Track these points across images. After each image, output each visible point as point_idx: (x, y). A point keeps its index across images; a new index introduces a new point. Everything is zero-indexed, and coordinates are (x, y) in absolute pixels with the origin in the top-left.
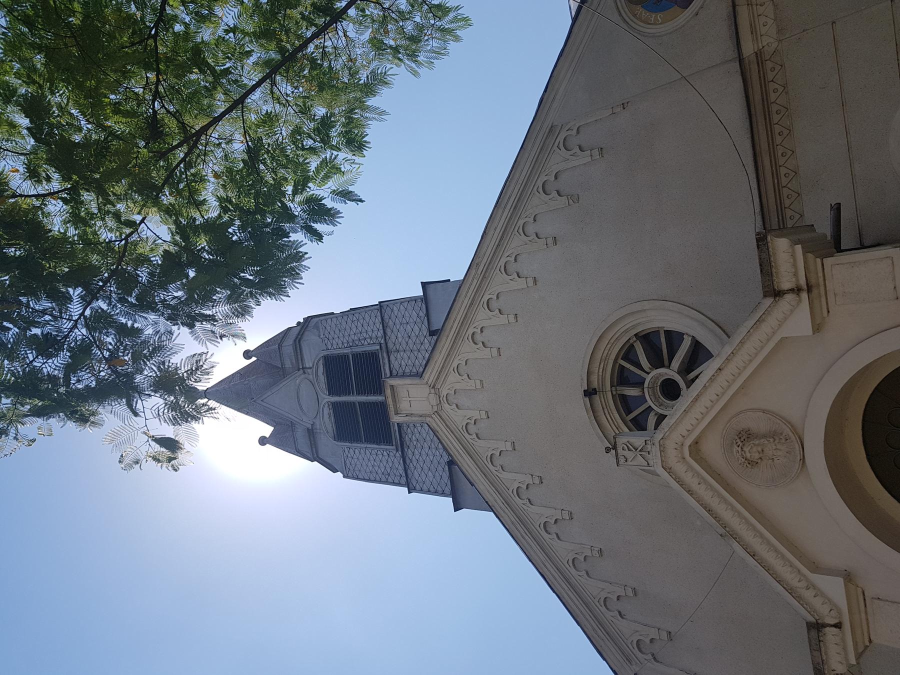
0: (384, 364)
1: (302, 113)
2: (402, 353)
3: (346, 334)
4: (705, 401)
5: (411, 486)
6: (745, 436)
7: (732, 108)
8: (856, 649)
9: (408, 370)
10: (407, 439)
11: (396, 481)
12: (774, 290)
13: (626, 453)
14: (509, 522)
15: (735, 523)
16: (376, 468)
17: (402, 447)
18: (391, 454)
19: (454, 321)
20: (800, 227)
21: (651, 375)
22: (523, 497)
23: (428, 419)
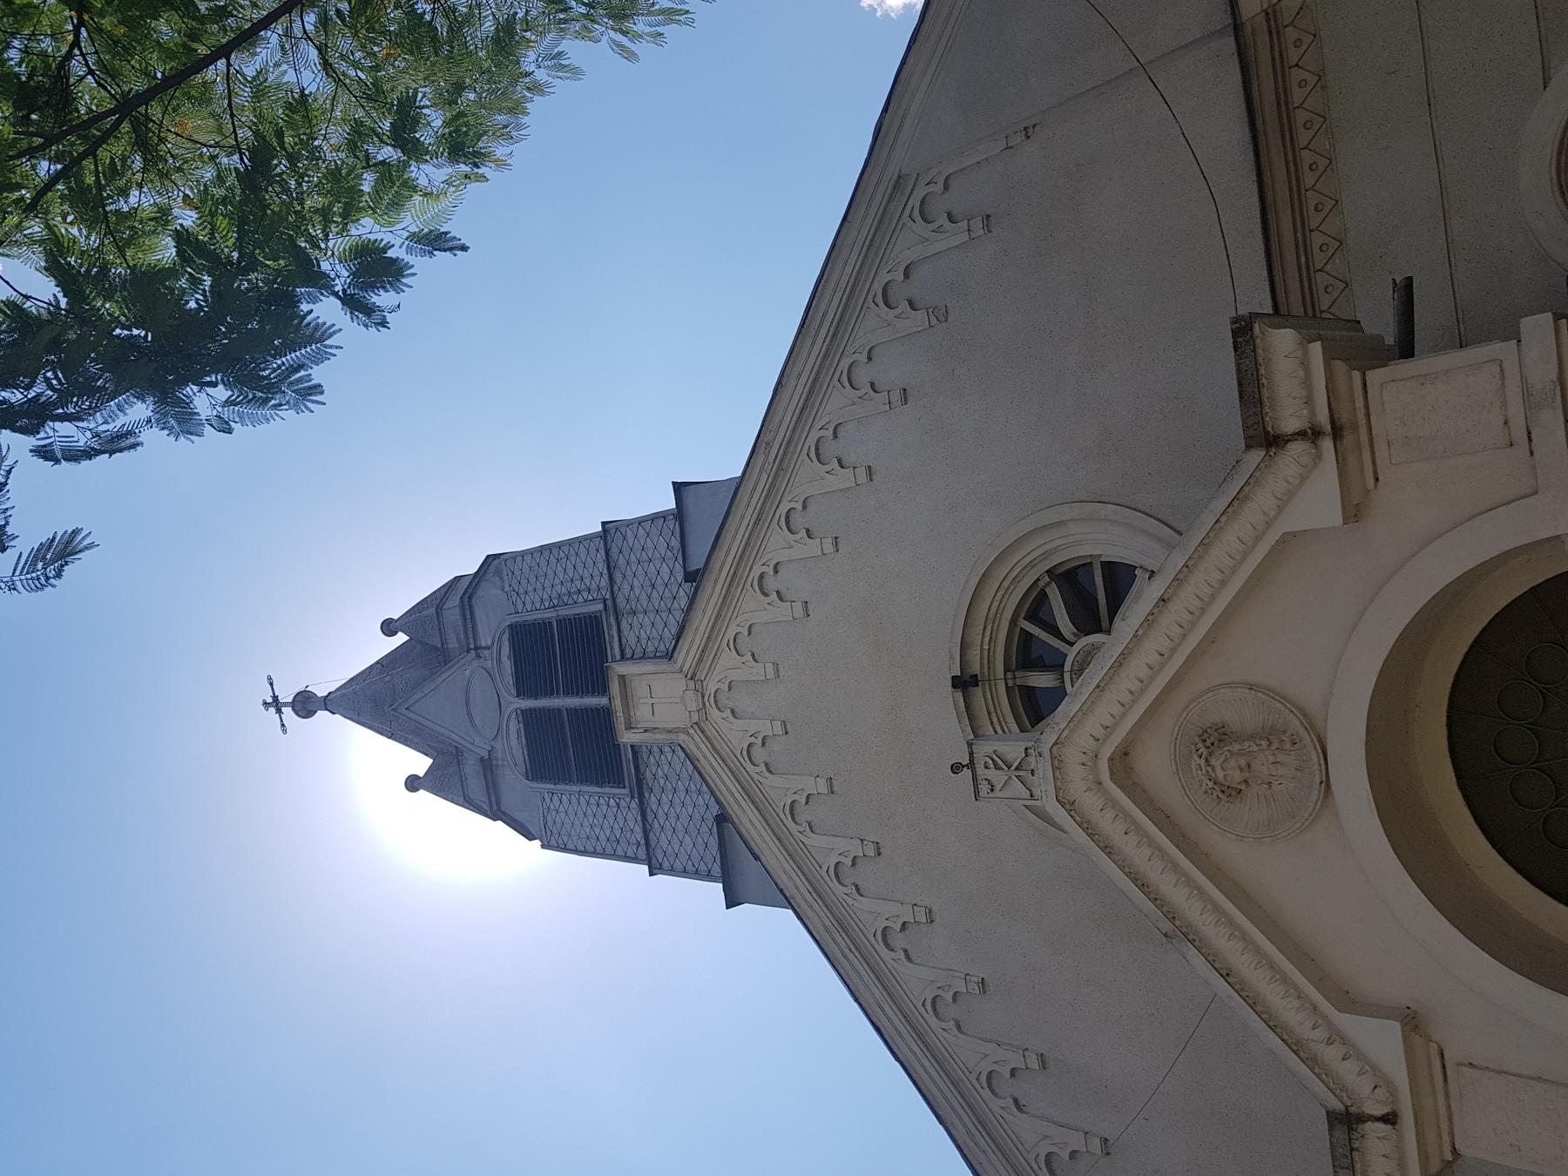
0: (611, 637)
1: (369, 98)
2: (641, 616)
3: (547, 584)
4: (1137, 667)
5: (654, 861)
6: (1216, 738)
7: (1220, 127)
9: (651, 648)
10: (648, 775)
11: (630, 854)
12: (1266, 433)
13: (992, 774)
14: (822, 930)
15: (1192, 911)
16: (597, 830)
17: (640, 790)
18: (623, 803)
19: (727, 554)
20: (1323, 313)
21: (1077, 648)
22: (848, 881)
23: (682, 737)
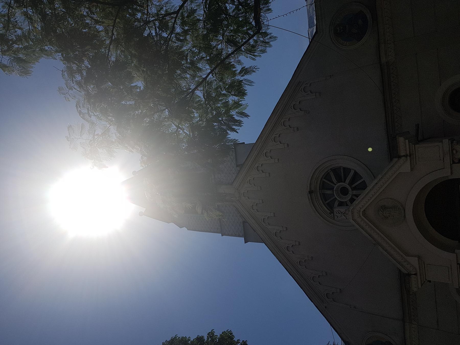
8: (421, 283)
13: (337, 215)
21: (337, 185)
